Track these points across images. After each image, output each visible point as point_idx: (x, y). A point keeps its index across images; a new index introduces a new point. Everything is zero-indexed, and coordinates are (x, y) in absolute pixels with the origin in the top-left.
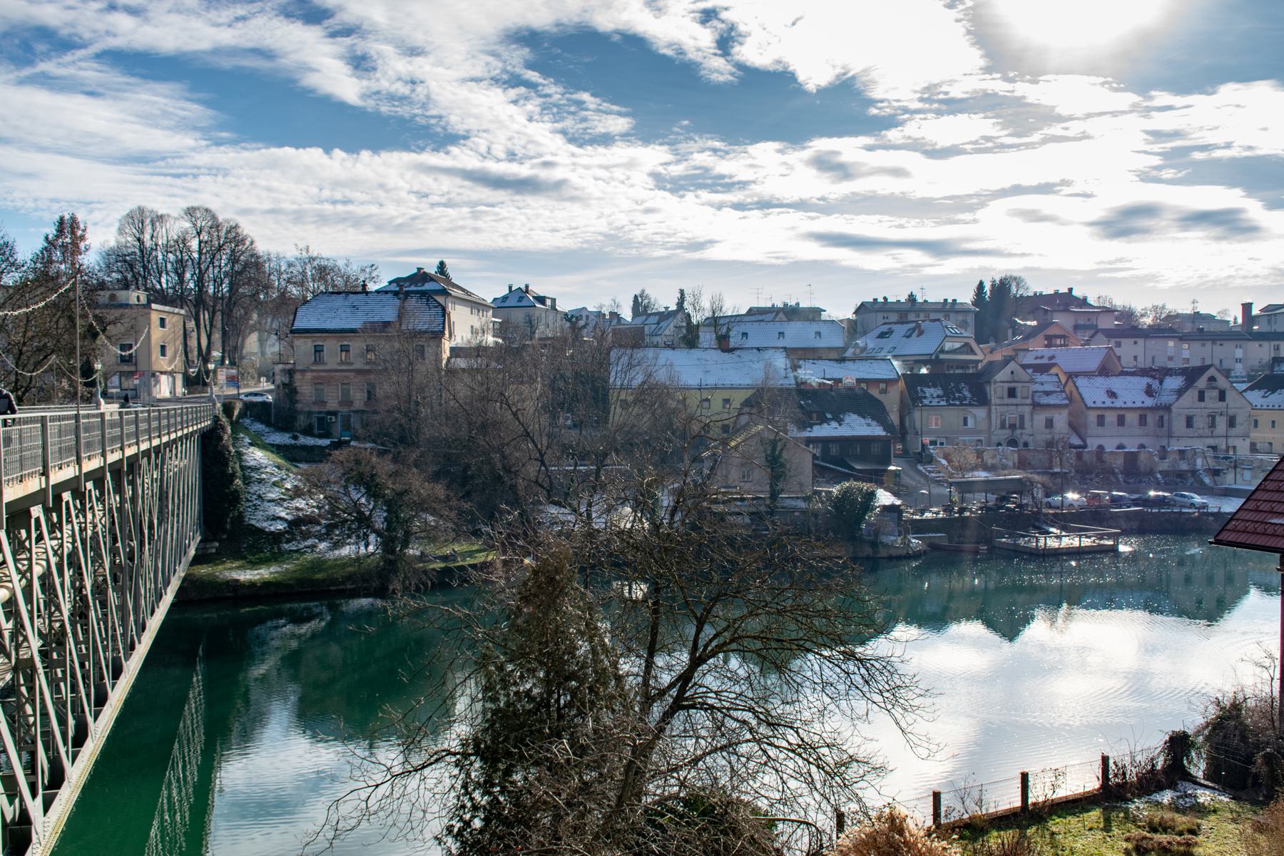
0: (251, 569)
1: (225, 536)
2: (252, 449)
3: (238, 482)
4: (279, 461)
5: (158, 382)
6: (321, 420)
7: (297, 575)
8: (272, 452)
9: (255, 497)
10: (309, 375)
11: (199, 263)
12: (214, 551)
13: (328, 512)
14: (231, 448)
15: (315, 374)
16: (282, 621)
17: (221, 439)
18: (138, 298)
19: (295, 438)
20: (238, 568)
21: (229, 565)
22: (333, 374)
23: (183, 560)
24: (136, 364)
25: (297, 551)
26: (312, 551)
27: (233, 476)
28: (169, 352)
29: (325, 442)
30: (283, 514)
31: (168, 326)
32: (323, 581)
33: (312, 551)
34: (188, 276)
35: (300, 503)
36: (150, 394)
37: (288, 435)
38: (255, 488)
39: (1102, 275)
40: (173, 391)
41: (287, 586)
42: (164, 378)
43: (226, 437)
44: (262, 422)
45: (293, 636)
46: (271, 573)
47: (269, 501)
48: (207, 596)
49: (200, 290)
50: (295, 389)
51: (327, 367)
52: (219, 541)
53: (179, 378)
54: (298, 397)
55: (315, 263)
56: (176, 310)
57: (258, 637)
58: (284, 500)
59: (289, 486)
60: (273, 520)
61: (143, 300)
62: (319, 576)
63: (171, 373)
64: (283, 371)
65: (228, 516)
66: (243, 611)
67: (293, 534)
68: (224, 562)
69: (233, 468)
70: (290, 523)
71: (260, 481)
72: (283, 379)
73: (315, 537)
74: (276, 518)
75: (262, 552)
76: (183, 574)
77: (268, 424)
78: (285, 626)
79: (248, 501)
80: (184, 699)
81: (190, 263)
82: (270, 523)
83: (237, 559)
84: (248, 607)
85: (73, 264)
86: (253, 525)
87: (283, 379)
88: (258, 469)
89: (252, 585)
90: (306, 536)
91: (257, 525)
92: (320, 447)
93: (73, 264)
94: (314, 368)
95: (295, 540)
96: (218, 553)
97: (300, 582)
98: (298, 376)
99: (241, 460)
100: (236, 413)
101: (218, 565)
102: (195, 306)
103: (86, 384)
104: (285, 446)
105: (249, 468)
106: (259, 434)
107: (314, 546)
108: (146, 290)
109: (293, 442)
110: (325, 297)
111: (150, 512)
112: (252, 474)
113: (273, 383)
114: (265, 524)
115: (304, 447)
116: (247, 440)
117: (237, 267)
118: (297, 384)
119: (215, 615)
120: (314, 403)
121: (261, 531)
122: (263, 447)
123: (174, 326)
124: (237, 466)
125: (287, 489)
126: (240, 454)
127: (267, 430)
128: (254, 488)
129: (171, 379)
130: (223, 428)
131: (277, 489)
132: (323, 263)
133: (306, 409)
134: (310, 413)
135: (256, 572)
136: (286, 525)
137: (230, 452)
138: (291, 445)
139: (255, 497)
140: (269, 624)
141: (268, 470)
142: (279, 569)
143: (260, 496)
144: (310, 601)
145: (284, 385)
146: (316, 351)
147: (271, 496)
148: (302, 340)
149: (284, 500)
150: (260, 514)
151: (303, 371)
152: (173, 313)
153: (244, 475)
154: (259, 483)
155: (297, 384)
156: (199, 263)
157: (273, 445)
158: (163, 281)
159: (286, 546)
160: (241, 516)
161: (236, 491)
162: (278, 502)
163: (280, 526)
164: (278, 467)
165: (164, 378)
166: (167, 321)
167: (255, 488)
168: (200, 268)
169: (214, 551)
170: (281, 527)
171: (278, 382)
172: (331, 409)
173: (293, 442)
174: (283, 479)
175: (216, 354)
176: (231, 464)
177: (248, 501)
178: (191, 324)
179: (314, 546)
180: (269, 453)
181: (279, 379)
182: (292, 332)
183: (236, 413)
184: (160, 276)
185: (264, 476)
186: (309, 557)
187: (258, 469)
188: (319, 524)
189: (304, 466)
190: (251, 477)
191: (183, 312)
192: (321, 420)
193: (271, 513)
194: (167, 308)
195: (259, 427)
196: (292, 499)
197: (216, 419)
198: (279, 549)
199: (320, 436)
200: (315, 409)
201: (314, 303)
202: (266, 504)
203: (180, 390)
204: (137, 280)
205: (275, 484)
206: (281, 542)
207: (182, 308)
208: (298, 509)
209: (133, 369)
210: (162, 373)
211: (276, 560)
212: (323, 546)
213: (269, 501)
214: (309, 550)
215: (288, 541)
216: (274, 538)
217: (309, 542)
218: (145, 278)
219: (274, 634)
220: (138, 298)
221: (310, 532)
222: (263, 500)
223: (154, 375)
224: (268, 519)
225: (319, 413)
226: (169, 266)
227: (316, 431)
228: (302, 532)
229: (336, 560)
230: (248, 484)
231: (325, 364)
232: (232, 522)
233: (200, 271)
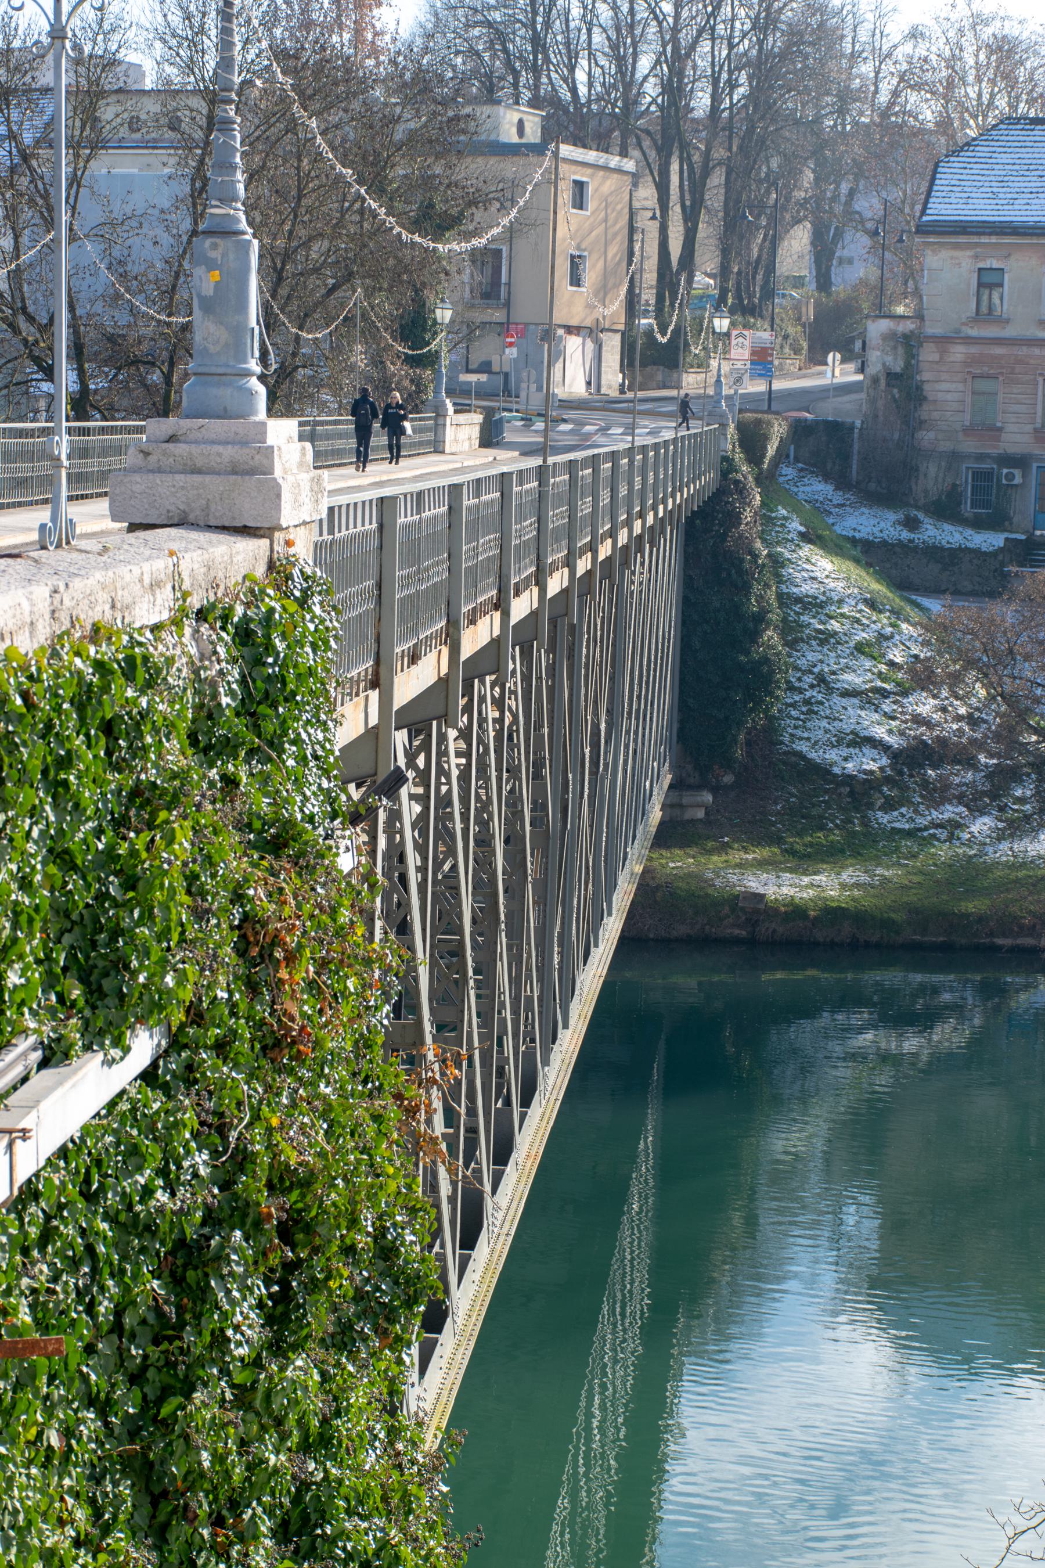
0: (791, 870)
1: (728, 779)
2: (806, 550)
3: (771, 636)
4: (875, 586)
5: (557, 354)
6: (982, 477)
7: (912, 898)
8: (857, 561)
9: (809, 679)
10: (958, 352)
11: (675, 30)
12: (700, 814)
13: (998, 737)
14: (758, 544)
15: (974, 350)
16: (856, 1020)
17: (734, 518)
18: (521, 124)
19: (912, 524)
20: (761, 864)
21: (736, 856)
22: (1024, 351)
23: (640, 828)
24: (508, 305)
25: (909, 834)
26: (951, 837)
27: (760, 619)
28: (591, 276)
29: (991, 540)
30: (880, 732)
31: (592, 204)
32: (981, 919)
33: (951, 837)
34: (645, 64)
35: (925, 705)
36: (544, 384)
37: (892, 516)
38: (811, 656)
39: (688, 203)
40: (593, 381)
41: (887, 924)
42: (573, 344)
43: (748, 515)
44: (827, 477)
45: (885, 1058)
46: (843, 886)
47: (846, 694)
48: (681, 930)
49: (673, 103)
50: (919, 388)
51: (1009, 332)
52: (715, 790)
53: (613, 345)
54: (925, 412)
55: (987, 33)
56: (614, 161)
57: (795, 1051)
58: (884, 694)
59: (897, 656)
60: (852, 744)
61: (533, 133)
62: (972, 906)
63: (592, 332)
64: (891, 337)
65: (740, 724)
66: (765, 977)
67: (904, 788)
68: (725, 848)
69: (760, 598)
70: (895, 755)
71: (826, 638)
72: (889, 359)
73: (960, 799)
74: (862, 741)
75: (822, 828)
76: (639, 869)
77: (842, 483)
78: (860, 1030)
79: (791, 688)
80: (622, 1197)
81: (653, 29)
82: (845, 752)
83: (758, 841)
84: (783, 966)
85: (358, 32)
86: (801, 755)
87: (889, 359)
88: (822, 606)
89: (796, 912)
90: (936, 795)
91: (812, 755)
92: (977, 552)
93: (358, 32)
94: (973, 332)
95: (909, 803)
96: (707, 822)
97: (920, 917)
98: (928, 354)
99: (780, 579)
100: (771, 450)
101: (710, 852)
102: (659, 150)
103: (413, 361)
104: (884, 543)
105: (798, 600)
106: (820, 509)
107: (954, 826)
108: (535, 103)
109: (906, 535)
110: (1016, 134)
111: (596, 702)
112: (805, 618)
113: (862, 370)
114: (832, 755)
115: (934, 552)
116: (796, 526)
117: (775, 41)
118: (926, 376)
119: (692, 982)
120: (968, 431)
121: (822, 771)
122: (834, 546)
123: (606, 203)
124: (771, 595)
125: (892, 664)
126: (777, 562)
127: (838, 498)
128: (810, 655)
129: (590, 345)
130: (741, 489)
131: (868, 664)
132: (1012, 29)
133: (945, 446)
134: (954, 457)
135: (806, 880)
136: (885, 761)
137: (755, 556)
138: (900, 544)
139: (809, 679)
140: (825, 1019)
141: (845, 610)
142: (864, 878)
143: (821, 679)
144: (824, 971)
145: (890, 375)
146: (980, 285)
147: (852, 679)
148: (945, 254)
149: (884, 694)
150: (819, 729)
151: (943, 341)
152: (605, 168)
153: (785, 620)
154: (822, 643)
155: (926, 376)
156: (675, 30)
157: (854, 541)
158: (581, 76)
159: (884, 818)
160: (771, 731)
161: (765, 660)
162: (871, 698)
163: (871, 763)
164: (871, 604)
165: (573, 344)
166: (590, 190)
167: (811, 656)
168: (675, 40)
169: (700, 814)
170: (873, 766)
171: (875, 367)
172: (1012, 449)
173: (906, 535)
174: (882, 637)
175: (703, 281)
176: (756, 587)
177: (791, 688)
178: (647, 194)
179: (954, 826)
180: (848, 565)
181: (877, 360)
182: (923, 230)
183: (771, 450)
184: (572, 69)
185: (834, 625)
186: (943, 852)
187: (822, 606)
188: (971, 763)
189: (935, 605)
190: (801, 626)
191: (629, 165)
192: (982, 477)
193: (848, 725)
194: (591, 156)
195: (819, 488)
196: (905, 693)
197: (727, 466)
198: (865, 823)
199: (978, 524)
200: (969, 446)
201: (982, 151)
202: (837, 701)
203: (612, 377)
204: (516, 74)
205: (860, 648)
206: (870, 806)
207: (624, 153)
208: (918, 720)
209: (499, 316)
210: (570, 330)
211: (857, 854)
212: (982, 826)
213: (846, 694)
214: (943, 834)
215: (889, 806)
216: (852, 793)
217: (950, 812)
218: (536, 71)
219: (836, 1048)
220: (521, 124)
221: (947, 786)
222: (830, 690)
223: (548, 335)
224: (839, 741)
225: (981, 457)
226: (598, 38)
227: (967, 509)
228: (925, 783)
229: (1012, 867)
230: (791, 645)
231: (1005, 321)
232: (749, 743)
233: (676, 49)
